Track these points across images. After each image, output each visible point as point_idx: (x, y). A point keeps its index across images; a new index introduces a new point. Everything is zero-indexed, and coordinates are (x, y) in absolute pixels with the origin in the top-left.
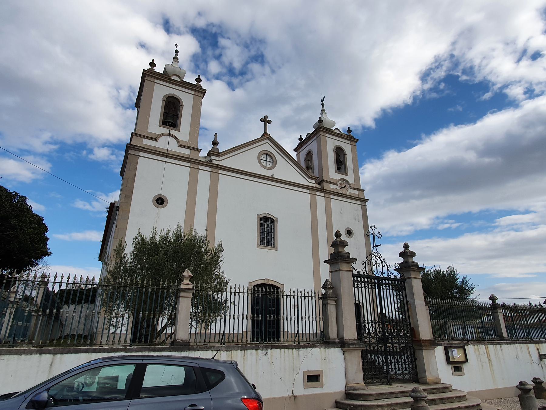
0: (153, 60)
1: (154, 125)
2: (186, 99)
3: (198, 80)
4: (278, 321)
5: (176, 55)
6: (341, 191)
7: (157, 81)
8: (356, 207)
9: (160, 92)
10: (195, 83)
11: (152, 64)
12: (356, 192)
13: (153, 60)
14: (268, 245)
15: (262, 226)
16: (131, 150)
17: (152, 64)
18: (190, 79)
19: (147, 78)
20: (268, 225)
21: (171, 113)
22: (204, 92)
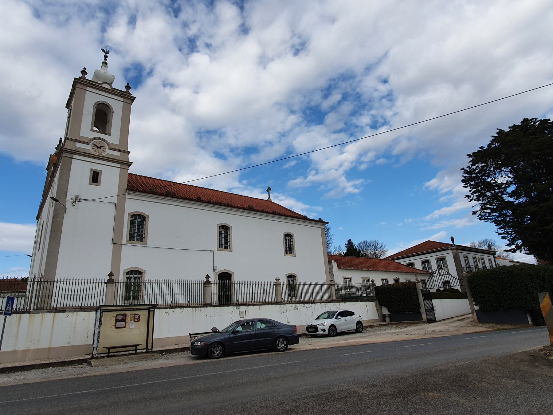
0: (85, 68)
1: (87, 130)
2: (116, 105)
3: (128, 87)
4: (219, 292)
5: (105, 59)
6: (93, 152)
7: (88, 89)
8: (317, 231)
9: (92, 98)
10: (125, 90)
11: (84, 72)
12: (117, 154)
13: (85, 68)
14: (225, 248)
15: (220, 233)
16: (62, 156)
17: (84, 72)
18: (119, 85)
19: (78, 85)
20: (225, 232)
21: (102, 116)
22: (133, 99)
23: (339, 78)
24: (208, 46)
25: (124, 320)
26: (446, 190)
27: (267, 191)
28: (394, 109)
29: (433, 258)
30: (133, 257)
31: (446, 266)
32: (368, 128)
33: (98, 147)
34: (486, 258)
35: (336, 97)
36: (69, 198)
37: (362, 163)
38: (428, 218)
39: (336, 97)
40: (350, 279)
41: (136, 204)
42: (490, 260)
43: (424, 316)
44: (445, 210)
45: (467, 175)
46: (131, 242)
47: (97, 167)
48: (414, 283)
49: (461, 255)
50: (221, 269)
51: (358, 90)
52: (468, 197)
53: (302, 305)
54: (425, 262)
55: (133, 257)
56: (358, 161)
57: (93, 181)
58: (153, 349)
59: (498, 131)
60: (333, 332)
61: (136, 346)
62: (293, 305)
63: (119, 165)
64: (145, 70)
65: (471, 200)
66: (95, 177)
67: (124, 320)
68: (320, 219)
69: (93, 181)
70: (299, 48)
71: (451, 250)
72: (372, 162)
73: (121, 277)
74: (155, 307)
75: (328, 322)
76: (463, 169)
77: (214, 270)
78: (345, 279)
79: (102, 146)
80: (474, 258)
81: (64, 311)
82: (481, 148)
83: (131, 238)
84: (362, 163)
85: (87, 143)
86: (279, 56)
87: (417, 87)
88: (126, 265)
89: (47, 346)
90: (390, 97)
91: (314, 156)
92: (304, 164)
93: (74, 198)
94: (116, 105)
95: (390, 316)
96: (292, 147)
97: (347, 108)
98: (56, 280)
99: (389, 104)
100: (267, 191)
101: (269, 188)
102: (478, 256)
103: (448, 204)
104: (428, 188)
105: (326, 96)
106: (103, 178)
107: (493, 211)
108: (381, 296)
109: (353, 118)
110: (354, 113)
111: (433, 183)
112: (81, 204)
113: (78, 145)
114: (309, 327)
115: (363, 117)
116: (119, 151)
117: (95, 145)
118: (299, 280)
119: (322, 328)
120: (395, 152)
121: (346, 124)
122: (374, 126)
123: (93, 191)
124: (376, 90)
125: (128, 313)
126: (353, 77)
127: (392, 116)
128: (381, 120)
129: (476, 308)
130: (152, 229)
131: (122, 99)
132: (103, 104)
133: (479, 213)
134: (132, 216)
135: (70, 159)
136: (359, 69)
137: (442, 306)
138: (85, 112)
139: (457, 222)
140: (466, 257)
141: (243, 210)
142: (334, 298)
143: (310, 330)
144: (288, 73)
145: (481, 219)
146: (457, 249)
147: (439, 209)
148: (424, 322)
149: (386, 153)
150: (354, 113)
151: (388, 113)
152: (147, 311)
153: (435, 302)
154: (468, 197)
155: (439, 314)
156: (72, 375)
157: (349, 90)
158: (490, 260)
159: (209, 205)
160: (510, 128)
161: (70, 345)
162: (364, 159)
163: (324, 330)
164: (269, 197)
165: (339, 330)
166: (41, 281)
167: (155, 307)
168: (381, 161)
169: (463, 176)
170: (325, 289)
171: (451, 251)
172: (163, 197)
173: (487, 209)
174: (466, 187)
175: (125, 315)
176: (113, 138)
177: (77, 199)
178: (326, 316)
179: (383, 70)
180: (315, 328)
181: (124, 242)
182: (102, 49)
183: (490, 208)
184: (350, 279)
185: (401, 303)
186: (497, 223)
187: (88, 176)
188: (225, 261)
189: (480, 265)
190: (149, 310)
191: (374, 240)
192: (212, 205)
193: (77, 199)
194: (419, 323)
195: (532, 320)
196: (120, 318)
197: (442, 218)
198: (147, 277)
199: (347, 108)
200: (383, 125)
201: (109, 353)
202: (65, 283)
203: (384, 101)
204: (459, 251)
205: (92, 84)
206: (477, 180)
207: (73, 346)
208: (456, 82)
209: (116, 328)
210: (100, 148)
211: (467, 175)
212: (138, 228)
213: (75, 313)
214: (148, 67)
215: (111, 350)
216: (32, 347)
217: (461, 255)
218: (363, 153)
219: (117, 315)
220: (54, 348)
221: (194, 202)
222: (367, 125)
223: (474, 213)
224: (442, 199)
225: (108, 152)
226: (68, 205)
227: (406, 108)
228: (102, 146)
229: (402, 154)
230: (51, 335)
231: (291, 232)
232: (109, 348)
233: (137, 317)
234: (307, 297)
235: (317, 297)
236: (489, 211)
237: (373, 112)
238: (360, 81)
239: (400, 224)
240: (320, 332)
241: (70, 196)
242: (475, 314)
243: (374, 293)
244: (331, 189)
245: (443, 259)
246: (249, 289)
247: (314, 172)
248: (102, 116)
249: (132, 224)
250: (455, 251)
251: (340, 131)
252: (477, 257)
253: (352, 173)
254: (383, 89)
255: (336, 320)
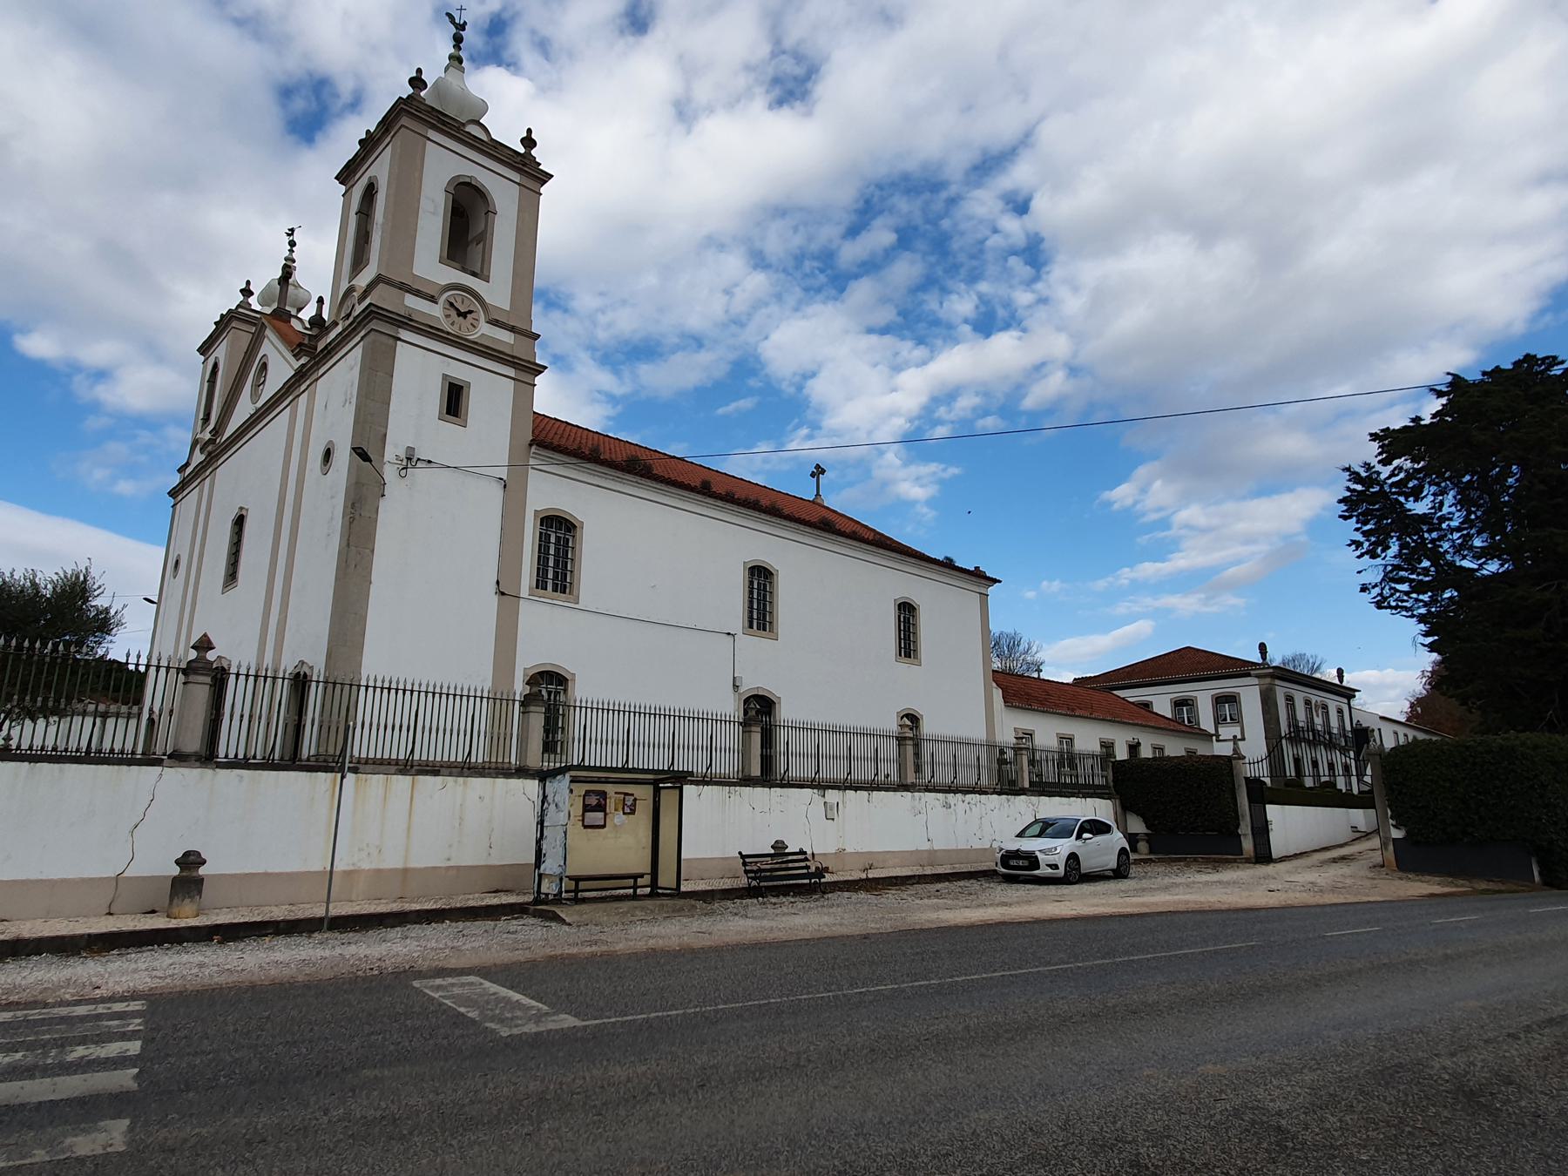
0: (419, 71)
2: (501, 189)
7: (432, 134)
10: (522, 150)
12: (506, 337)
21: (467, 218)
23: (893, 184)
24: (543, 46)
25: (601, 807)
26: (1154, 516)
27: (813, 475)
28: (1039, 286)
29: (1203, 695)
30: (547, 634)
31: (1237, 719)
32: (967, 328)
33: (460, 314)
34: (1333, 703)
35: (881, 236)
36: (389, 454)
37: (940, 422)
38: (1101, 584)
39: (881, 236)
41: (553, 489)
42: (1340, 711)
43: (1248, 845)
44: (1148, 569)
45: (1359, 487)
46: (542, 592)
47: (460, 373)
48: (1229, 759)
49: (1281, 690)
50: (749, 685)
51: (946, 224)
52: (1358, 544)
53: (959, 796)
54: (1179, 704)
55: (547, 634)
56: (927, 415)
57: (448, 413)
58: (683, 889)
59: (1450, 378)
60: (1074, 874)
62: (940, 796)
63: (511, 372)
64: (337, 96)
65: (1362, 555)
66: (454, 400)
67: (601, 807)
68: (977, 568)
69: (448, 413)
70: (792, 84)
71: (1258, 676)
72: (964, 422)
74: (680, 779)
75: (1064, 847)
76: (1348, 469)
77: (736, 687)
79: (471, 312)
80: (1308, 702)
81: (436, 773)
82: (1413, 420)
83: (541, 584)
84: (940, 422)
85: (432, 299)
86: (734, 102)
87: (1107, 234)
89: (400, 865)
90: (1035, 254)
91: (818, 389)
92: (786, 406)
93: (403, 456)
94: (501, 189)
95: (1149, 839)
96: (757, 358)
97: (906, 270)
98: (363, 683)
99: (1024, 271)
100: (813, 475)
101: (818, 466)
102: (1316, 697)
103: (1161, 551)
104: (1109, 504)
105: (853, 232)
106: (475, 402)
107: (1418, 587)
108: (1130, 783)
109: (926, 297)
110: (928, 283)
111: (1123, 493)
112: (419, 474)
113: (411, 302)
114: (1009, 857)
115: (954, 297)
116: (512, 329)
117: (452, 304)
118: (927, 728)
119: (1051, 859)
120: (1029, 403)
121: (903, 313)
122: (986, 324)
123: (440, 439)
124: (995, 231)
125: (610, 789)
126: (936, 186)
127: (1029, 307)
128: (1001, 313)
129: (1397, 834)
130: (593, 559)
131: (516, 177)
132: (469, 184)
133: (1377, 590)
135: (391, 341)
136: (956, 166)
137: (1290, 824)
138: (425, 204)
139: (1173, 600)
140: (1290, 699)
141: (808, 529)
142: (984, 781)
143: (1013, 863)
144: (760, 153)
145: (1379, 605)
146: (1272, 676)
147: (1131, 566)
148: (1248, 861)
149: (1005, 400)
150: (928, 283)
151: (1023, 298)
152: (650, 788)
153: (1273, 811)
154: (1358, 544)
155: (1279, 842)
157: (918, 219)
158: (1340, 711)
159: (728, 506)
160: (1484, 373)
161: (451, 863)
162: (942, 412)
163: (1055, 867)
164: (818, 494)
165: (1086, 866)
166: (326, 682)
167: (680, 779)
168: (990, 423)
169: (1348, 489)
170: (890, 749)
171: (1256, 681)
172: (619, 474)
173: (1402, 580)
174: (1345, 518)
175: (603, 794)
176: (497, 291)
177: (410, 460)
178: (1036, 829)
179: (1021, 174)
180: (1032, 860)
181: (524, 592)
182: (448, 15)
183: (1411, 581)
185: (1185, 808)
186: (1422, 619)
187: (435, 398)
189: (1318, 721)
190: (655, 783)
191: (1009, 630)
192: (735, 508)
193: (410, 460)
194: (1235, 861)
195: (1540, 873)
196: (593, 801)
197: (1138, 587)
199: (906, 270)
200: (1006, 326)
201: (576, 891)
202: (242, 678)
203: (1013, 261)
204: (1277, 682)
205: (444, 123)
206: (1372, 507)
207: (458, 868)
208: (1207, 232)
209: (585, 827)
210: (463, 315)
211: (1359, 487)
213: (461, 780)
214: (346, 87)
215: (582, 885)
216: (366, 866)
217: (1281, 690)
218: (947, 395)
219: (588, 793)
220: (415, 870)
221: (692, 495)
222: (966, 321)
223: (1364, 589)
224: (1143, 540)
225: (484, 331)
226: (390, 473)
227: (1075, 283)
228: (471, 312)
229: (1051, 409)
230: (408, 837)
231: (916, 599)
232: (577, 879)
233: (629, 801)
234: (944, 776)
235: (864, 772)
236: (1405, 587)
237: (983, 287)
238: (953, 201)
239: (1031, 594)
240: (1044, 871)
241: (393, 450)
242: (1391, 847)
243: (1111, 777)
244: (851, 484)
245: (1232, 699)
246: (402, 710)
247: (804, 431)
248: (467, 218)
249: (544, 541)
250: (1268, 680)
251: (884, 331)
252: (1314, 699)
253: (914, 442)
254: (1013, 226)
255: (1079, 843)
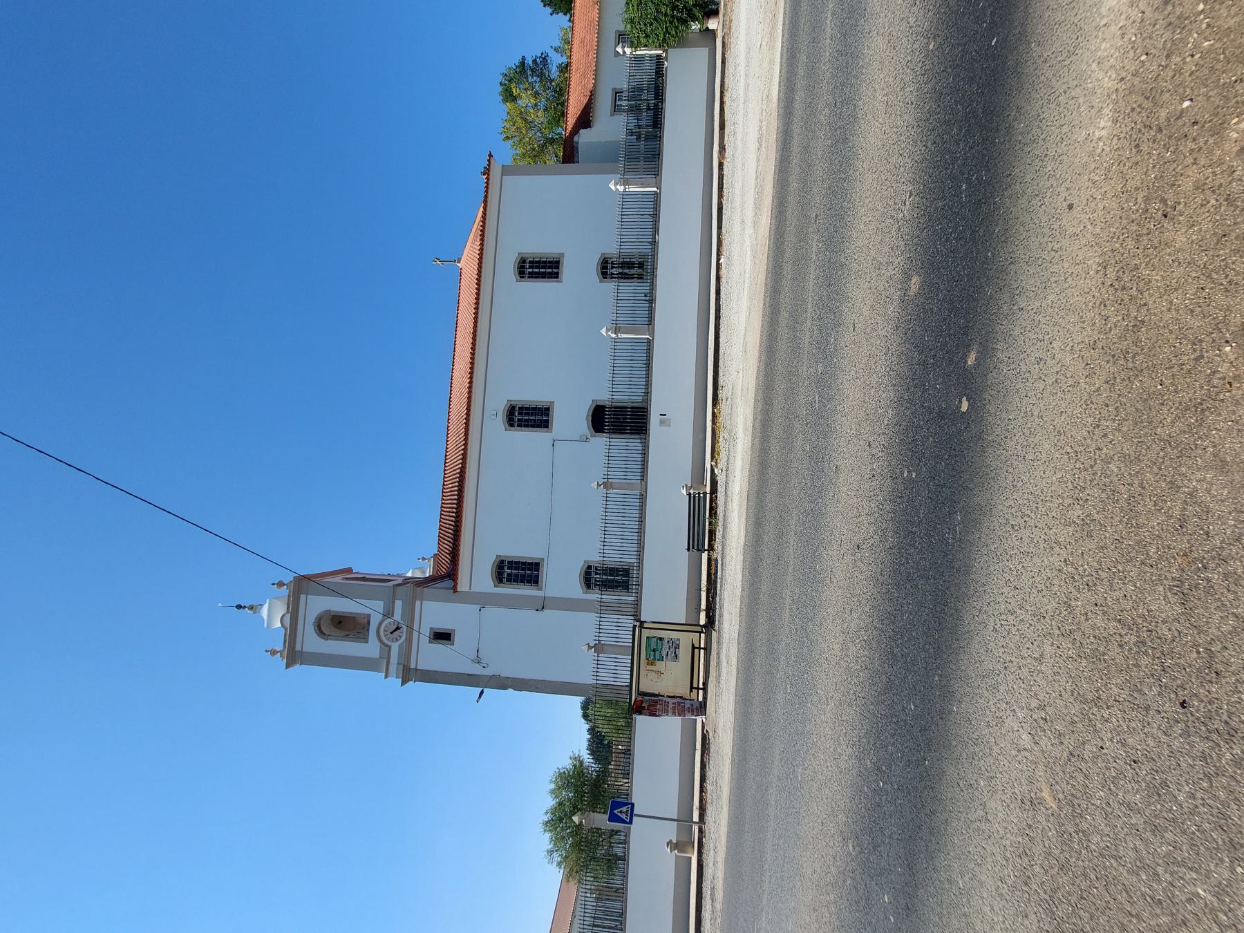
15: (533, 276)
30: (562, 578)
40: (617, 94)
41: (476, 573)
61: (694, 648)
66: (442, 636)
73: (594, 596)
78: (616, 109)
88: (575, 589)
106: (442, 626)
132: (319, 626)
134: (501, 581)
156: (774, 27)
176: (372, 608)
184: (617, 94)
187: (440, 647)
188: (571, 418)
191: (500, 78)
198: (595, 558)
212: (519, 573)
249: (513, 579)
